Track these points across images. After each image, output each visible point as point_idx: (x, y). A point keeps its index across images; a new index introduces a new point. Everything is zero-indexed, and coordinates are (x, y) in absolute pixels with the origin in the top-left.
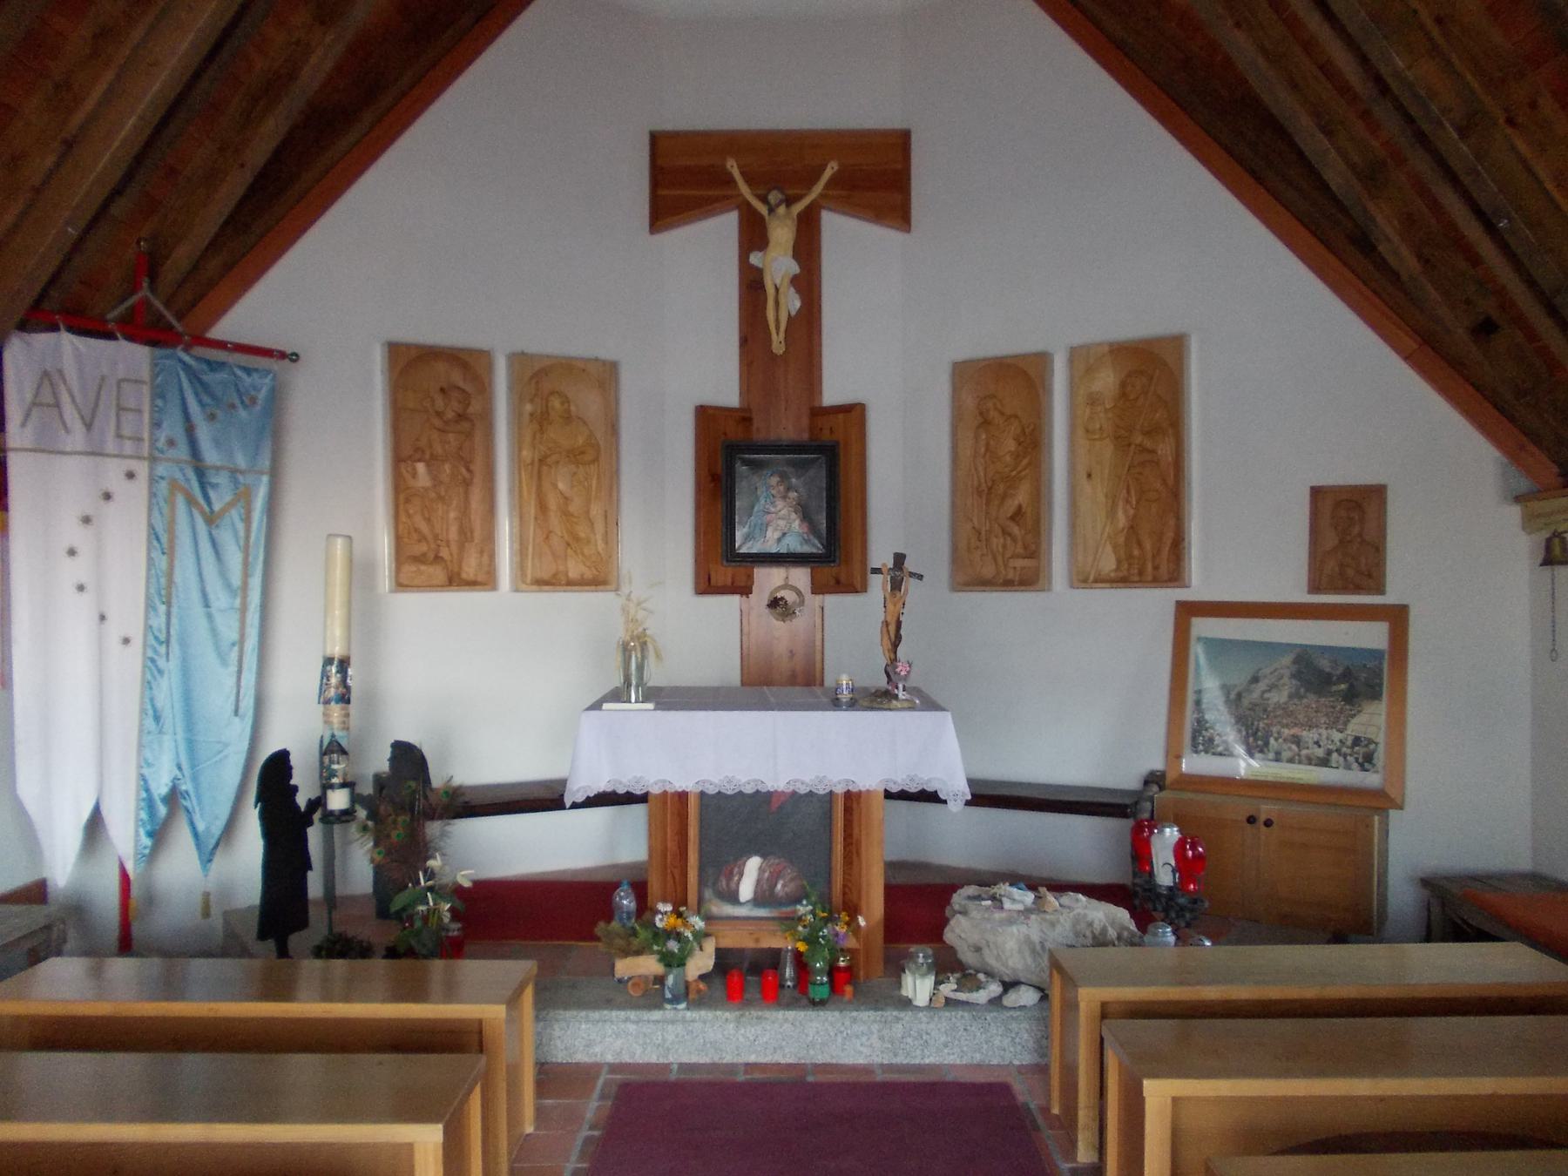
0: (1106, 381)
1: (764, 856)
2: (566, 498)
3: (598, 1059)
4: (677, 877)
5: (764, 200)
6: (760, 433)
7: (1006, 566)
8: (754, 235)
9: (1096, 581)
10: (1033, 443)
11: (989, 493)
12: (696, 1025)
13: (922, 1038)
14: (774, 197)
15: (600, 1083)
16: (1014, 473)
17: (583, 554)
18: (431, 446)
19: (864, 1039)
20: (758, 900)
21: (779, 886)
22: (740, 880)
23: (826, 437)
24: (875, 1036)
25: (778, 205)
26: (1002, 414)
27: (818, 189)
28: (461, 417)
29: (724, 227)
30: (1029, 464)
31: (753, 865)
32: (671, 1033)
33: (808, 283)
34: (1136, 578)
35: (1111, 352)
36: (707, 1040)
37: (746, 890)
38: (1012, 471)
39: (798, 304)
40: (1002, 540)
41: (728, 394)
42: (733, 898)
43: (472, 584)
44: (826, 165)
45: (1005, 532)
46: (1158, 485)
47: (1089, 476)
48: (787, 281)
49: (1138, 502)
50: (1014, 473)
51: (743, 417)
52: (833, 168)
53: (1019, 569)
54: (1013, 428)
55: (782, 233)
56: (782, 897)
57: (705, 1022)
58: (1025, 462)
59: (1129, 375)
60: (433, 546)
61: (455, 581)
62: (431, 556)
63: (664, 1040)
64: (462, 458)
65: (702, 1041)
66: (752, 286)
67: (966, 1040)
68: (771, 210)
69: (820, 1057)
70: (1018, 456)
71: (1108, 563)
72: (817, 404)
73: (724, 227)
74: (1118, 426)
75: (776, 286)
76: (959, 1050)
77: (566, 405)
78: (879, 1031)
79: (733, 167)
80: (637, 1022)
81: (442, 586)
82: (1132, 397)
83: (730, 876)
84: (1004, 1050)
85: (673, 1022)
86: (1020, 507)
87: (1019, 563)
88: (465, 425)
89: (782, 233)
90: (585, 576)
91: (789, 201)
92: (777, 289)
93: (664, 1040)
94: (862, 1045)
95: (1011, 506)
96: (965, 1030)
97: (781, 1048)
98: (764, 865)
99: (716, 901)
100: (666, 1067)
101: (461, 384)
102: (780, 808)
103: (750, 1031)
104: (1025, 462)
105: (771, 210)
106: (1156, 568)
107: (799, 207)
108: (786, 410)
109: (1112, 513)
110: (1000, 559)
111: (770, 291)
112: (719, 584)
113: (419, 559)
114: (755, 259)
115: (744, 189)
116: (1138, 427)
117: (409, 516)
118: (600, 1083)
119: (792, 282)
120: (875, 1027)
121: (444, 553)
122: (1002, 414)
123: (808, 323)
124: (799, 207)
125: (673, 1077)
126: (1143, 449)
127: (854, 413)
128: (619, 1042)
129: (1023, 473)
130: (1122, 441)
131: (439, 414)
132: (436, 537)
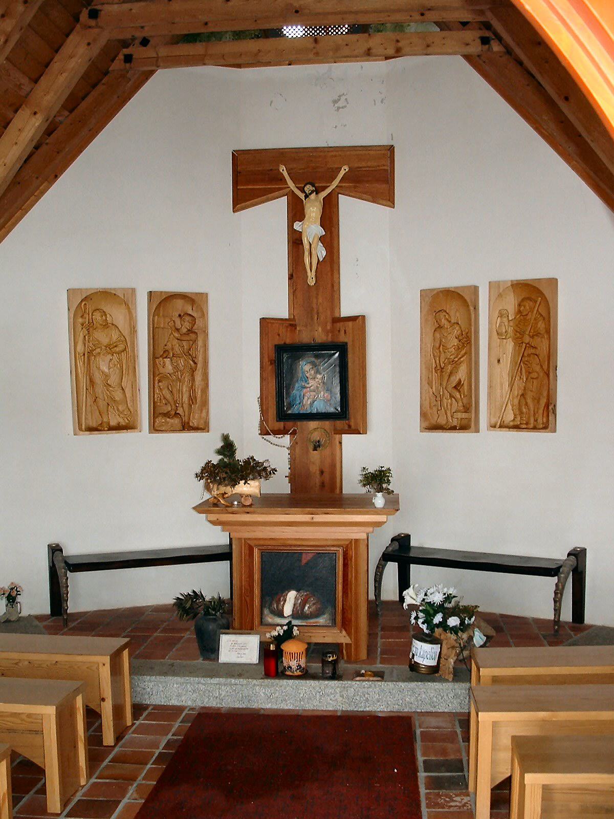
0: (510, 304)
1: (298, 591)
2: (106, 376)
3: (184, 704)
4: (248, 602)
5: (303, 191)
6: (304, 336)
7: (452, 417)
8: (296, 212)
9: (501, 427)
10: (468, 340)
11: (442, 372)
12: (237, 686)
13: (365, 696)
14: (308, 188)
15: (184, 714)
16: (456, 359)
17: (118, 410)
18: (173, 349)
19: (332, 696)
20: (295, 615)
21: (306, 608)
22: (284, 604)
23: (342, 338)
24: (338, 695)
25: (310, 194)
26: (450, 322)
27: (336, 183)
28: (190, 331)
29: (278, 207)
30: (466, 353)
31: (292, 595)
32: (224, 691)
33: (330, 239)
34: (524, 426)
35: (512, 285)
36: (244, 695)
37: (288, 610)
38: (455, 358)
39: (324, 253)
40: (450, 401)
41: (281, 309)
42: (280, 614)
43: (196, 429)
44: (341, 168)
45: (451, 396)
46: (538, 368)
47: (499, 361)
48: (316, 239)
49: (527, 379)
50: (456, 359)
51: (290, 324)
52: (345, 170)
53: (459, 419)
54: (456, 331)
55: (313, 209)
56: (308, 614)
57: (242, 685)
58: (463, 352)
59: (523, 300)
60: (174, 407)
61: (186, 427)
62: (173, 413)
63: (220, 695)
64: (190, 355)
65: (241, 696)
66: (296, 241)
67: (390, 698)
68: (306, 196)
69: (307, 706)
70: (459, 349)
71: (509, 417)
72: (337, 315)
73: (278, 207)
74: (517, 331)
75: (310, 243)
76: (386, 704)
77: (104, 317)
78: (340, 692)
79: (283, 169)
80: (204, 684)
81: (181, 430)
82: (524, 314)
83: (278, 602)
84: (411, 703)
85: (225, 685)
86: (460, 381)
87: (459, 415)
88: (193, 336)
89: (313, 209)
90: (121, 424)
91: (317, 191)
92: (310, 245)
93: (220, 695)
94: (331, 699)
95: (454, 380)
96: (390, 692)
97: (285, 700)
98: (298, 596)
99: (271, 615)
100: (336, 711)
101: (190, 312)
102: (307, 563)
103: (268, 691)
104: (463, 352)
105: (306, 196)
106: (536, 420)
107: (324, 194)
108: (317, 319)
109: (511, 386)
110: (449, 413)
111: (306, 246)
112: (275, 429)
113: (167, 415)
114: (297, 226)
115: (290, 183)
116: (527, 333)
117: (161, 389)
118: (184, 714)
119: (320, 239)
120: (338, 690)
121: (180, 411)
122: (450, 322)
123: (331, 264)
124: (324, 194)
125: (339, 714)
126: (529, 345)
127: (358, 321)
128: (195, 695)
129: (462, 359)
130: (518, 338)
131: (178, 330)
132: (175, 402)
